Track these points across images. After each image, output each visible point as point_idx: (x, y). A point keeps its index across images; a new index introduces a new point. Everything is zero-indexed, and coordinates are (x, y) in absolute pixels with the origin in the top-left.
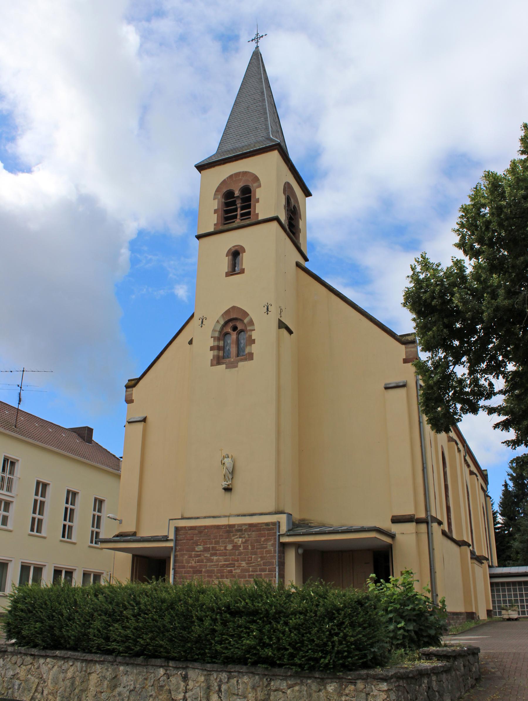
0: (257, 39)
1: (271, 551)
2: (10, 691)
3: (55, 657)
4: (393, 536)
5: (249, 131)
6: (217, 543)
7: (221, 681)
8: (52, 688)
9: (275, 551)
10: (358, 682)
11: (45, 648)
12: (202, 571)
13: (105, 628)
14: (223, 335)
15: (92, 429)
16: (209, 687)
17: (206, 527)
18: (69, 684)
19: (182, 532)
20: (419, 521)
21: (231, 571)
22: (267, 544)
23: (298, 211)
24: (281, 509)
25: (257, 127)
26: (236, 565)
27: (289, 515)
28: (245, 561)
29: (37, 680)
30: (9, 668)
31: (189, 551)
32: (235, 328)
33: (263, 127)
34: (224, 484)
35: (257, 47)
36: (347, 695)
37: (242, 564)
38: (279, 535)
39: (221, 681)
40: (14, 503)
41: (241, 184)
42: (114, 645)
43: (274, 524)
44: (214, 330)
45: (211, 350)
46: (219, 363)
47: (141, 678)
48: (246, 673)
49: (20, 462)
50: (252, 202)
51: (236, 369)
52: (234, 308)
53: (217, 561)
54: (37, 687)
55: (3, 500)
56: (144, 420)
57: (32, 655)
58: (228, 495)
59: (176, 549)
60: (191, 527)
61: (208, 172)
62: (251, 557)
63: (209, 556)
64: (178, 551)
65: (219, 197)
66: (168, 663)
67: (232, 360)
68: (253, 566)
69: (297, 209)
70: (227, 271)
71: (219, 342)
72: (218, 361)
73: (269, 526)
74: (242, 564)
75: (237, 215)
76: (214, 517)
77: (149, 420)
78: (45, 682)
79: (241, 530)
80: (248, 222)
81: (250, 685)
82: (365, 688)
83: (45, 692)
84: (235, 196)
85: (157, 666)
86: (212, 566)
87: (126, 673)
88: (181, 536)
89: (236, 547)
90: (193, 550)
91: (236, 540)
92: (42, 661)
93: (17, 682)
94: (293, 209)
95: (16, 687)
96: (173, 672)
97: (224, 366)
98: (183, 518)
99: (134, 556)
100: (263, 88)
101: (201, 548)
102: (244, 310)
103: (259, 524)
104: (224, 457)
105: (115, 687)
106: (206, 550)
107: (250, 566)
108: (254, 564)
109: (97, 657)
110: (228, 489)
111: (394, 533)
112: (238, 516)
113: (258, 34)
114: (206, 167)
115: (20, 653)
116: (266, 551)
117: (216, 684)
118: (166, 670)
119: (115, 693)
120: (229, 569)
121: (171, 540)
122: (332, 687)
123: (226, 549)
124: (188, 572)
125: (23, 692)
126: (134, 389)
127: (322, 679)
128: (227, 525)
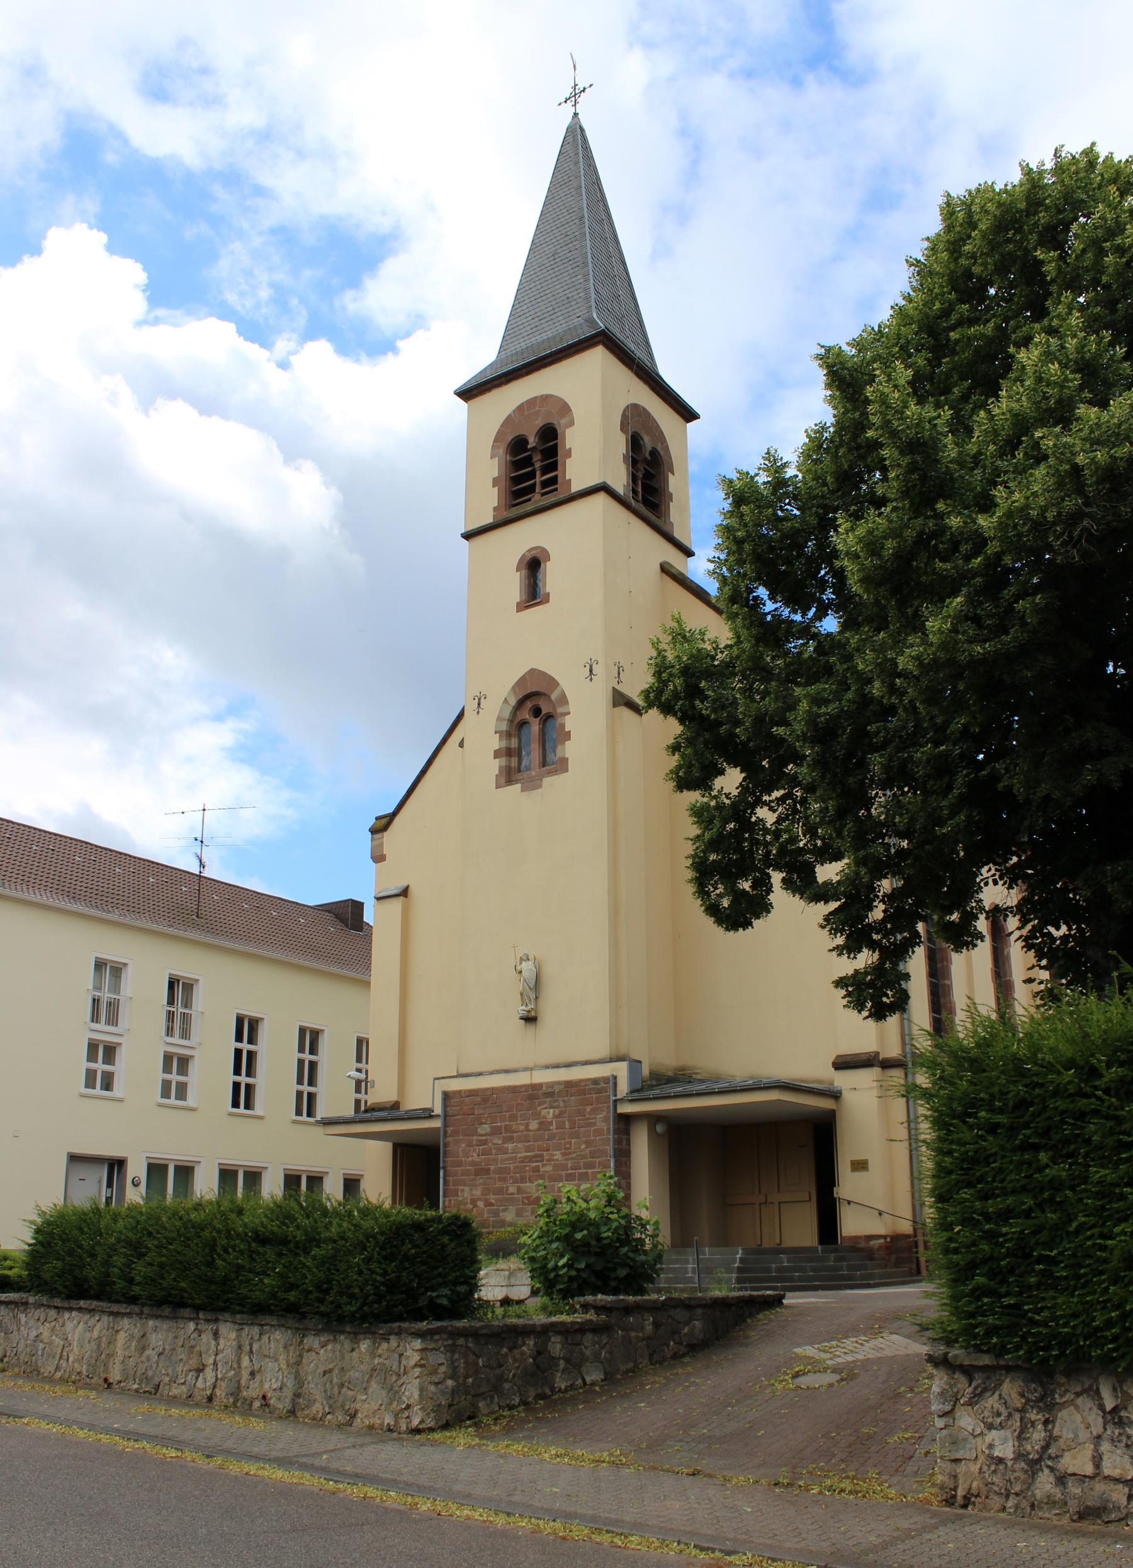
0: (575, 95)
1: (603, 1130)
2: (34, 1358)
3: (80, 1309)
4: (836, 1096)
5: (556, 306)
6: (513, 1118)
7: (252, 1338)
8: (77, 1353)
9: (608, 1129)
10: (392, 1337)
11: (69, 1297)
12: (489, 1169)
13: (128, 1266)
14: (516, 727)
15: (362, 904)
16: (240, 1347)
17: (493, 1090)
18: (95, 1347)
19: (454, 1101)
20: (887, 1065)
21: (537, 1169)
22: (595, 1118)
23: (664, 458)
24: (623, 1051)
25: (570, 295)
26: (546, 1157)
27: (635, 1064)
28: (559, 1149)
29: (62, 1343)
30: (32, 1327)
31: (468, 1135)
32: (537, 712)
33: (581, 295)
34: (521, 1010)
35: (576, 114)
36: (380, 1356)
37: (555, 1155)
38: (615, 1101)
39: (252, 1338)
40: (196, 1059)
41: (540, 423)
42: (137, 1290)
43: (606, 1080)
44: (499, 719)
45: (495, 757)
46: (510, 781)
47: (171, 1336)
48: (278, 1326)
49: (201, 983)
50: (559, 458)
51: (539, 791)
52: (532, 672)
53: (514, 1151)
54: (62, 1352)
55: (176, 1054)
56: (405, 893)
57: (56, 1307)
58: (531, 1028)
59: (445, 1132)
60: (470, 1091)
61: (485, 401)
62: (570, 1143)
63: (500, 1142)
64: (450, 1136)
65: (501, 451)
66: (198, 1314)
67: (534, 774)
68: (573, 1159)
69: (662, 453)
70: (518, 600)
71: (510, 739)
72: (509, 776)
73: (598, 1084)
74: (555, 1155)
75: (534, 484)
76: (507, 1071)
77: (412, 891)
78: (70, 1344)
79: (551, 1094)
80: (552, 498)
81: (282, 1343)
82: (398, 1346)
83: (71, 1359)
84: (529, 447)
85: (186, 1318)
86: (506, 1160)
87: (155, 1329)
88: (454, 1108)
89: (544, 1125)
90: (475, 1133)
91: (544, 1112)
92: (67, 1315)
93: (41, 1346)
94: (649, 458)
95: (40, 1353)
96: (203, 1326)
97: (518, 786)
98: (460, 1076)
99: (396, 1146)
100: (581, 209)
101: (486, 1128)
102: (550, 676)
103: (581, 1081)
104: (521, 960)
105: (144, 1348)
106: (496, 1131)
107: (567, 1159)
108: (574, 1155)
109: (123, 1308)
110: (530, 1019)
111: (839, 1089)
112: (547, 1067)
113: (576, 85)
114: (475, 392)
115: (43, 1305)
116: (595, 1131)
117: (247, 1342)
118: (197, 1325)
119: (144, 1358)
120: (534, 1164)
121: (438, 1116)
122: (365, 1346)
123: (528, 1130)
124: (466, 1173)
125: (47, 1360)
126: (386, 834)
127: (356, 1334)
128: (528, 1086)
